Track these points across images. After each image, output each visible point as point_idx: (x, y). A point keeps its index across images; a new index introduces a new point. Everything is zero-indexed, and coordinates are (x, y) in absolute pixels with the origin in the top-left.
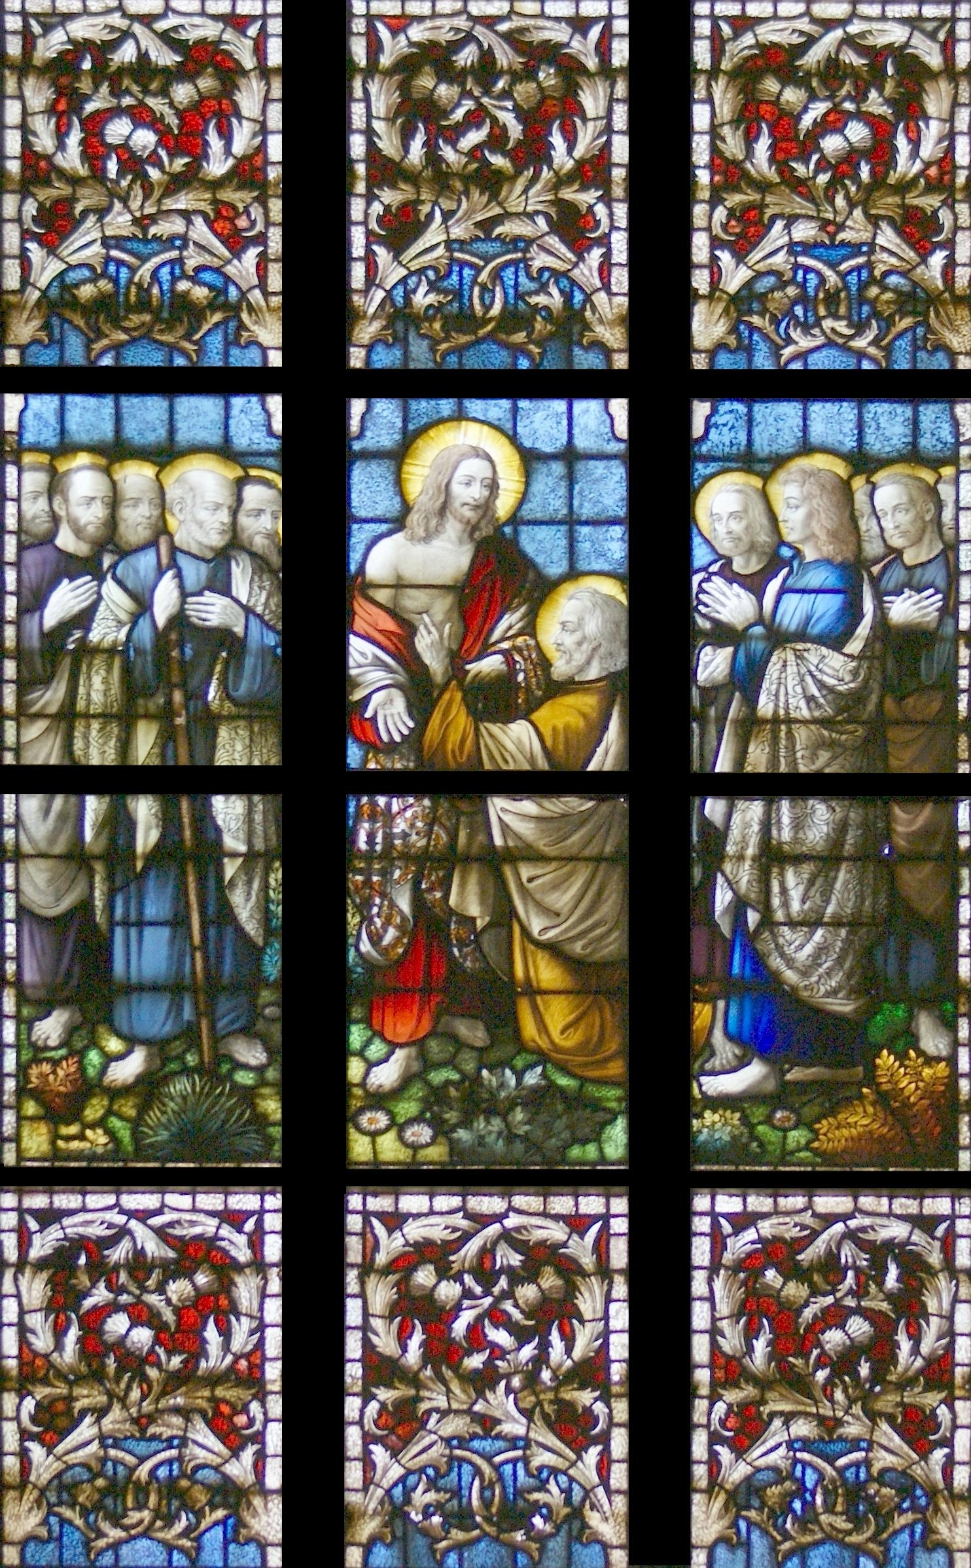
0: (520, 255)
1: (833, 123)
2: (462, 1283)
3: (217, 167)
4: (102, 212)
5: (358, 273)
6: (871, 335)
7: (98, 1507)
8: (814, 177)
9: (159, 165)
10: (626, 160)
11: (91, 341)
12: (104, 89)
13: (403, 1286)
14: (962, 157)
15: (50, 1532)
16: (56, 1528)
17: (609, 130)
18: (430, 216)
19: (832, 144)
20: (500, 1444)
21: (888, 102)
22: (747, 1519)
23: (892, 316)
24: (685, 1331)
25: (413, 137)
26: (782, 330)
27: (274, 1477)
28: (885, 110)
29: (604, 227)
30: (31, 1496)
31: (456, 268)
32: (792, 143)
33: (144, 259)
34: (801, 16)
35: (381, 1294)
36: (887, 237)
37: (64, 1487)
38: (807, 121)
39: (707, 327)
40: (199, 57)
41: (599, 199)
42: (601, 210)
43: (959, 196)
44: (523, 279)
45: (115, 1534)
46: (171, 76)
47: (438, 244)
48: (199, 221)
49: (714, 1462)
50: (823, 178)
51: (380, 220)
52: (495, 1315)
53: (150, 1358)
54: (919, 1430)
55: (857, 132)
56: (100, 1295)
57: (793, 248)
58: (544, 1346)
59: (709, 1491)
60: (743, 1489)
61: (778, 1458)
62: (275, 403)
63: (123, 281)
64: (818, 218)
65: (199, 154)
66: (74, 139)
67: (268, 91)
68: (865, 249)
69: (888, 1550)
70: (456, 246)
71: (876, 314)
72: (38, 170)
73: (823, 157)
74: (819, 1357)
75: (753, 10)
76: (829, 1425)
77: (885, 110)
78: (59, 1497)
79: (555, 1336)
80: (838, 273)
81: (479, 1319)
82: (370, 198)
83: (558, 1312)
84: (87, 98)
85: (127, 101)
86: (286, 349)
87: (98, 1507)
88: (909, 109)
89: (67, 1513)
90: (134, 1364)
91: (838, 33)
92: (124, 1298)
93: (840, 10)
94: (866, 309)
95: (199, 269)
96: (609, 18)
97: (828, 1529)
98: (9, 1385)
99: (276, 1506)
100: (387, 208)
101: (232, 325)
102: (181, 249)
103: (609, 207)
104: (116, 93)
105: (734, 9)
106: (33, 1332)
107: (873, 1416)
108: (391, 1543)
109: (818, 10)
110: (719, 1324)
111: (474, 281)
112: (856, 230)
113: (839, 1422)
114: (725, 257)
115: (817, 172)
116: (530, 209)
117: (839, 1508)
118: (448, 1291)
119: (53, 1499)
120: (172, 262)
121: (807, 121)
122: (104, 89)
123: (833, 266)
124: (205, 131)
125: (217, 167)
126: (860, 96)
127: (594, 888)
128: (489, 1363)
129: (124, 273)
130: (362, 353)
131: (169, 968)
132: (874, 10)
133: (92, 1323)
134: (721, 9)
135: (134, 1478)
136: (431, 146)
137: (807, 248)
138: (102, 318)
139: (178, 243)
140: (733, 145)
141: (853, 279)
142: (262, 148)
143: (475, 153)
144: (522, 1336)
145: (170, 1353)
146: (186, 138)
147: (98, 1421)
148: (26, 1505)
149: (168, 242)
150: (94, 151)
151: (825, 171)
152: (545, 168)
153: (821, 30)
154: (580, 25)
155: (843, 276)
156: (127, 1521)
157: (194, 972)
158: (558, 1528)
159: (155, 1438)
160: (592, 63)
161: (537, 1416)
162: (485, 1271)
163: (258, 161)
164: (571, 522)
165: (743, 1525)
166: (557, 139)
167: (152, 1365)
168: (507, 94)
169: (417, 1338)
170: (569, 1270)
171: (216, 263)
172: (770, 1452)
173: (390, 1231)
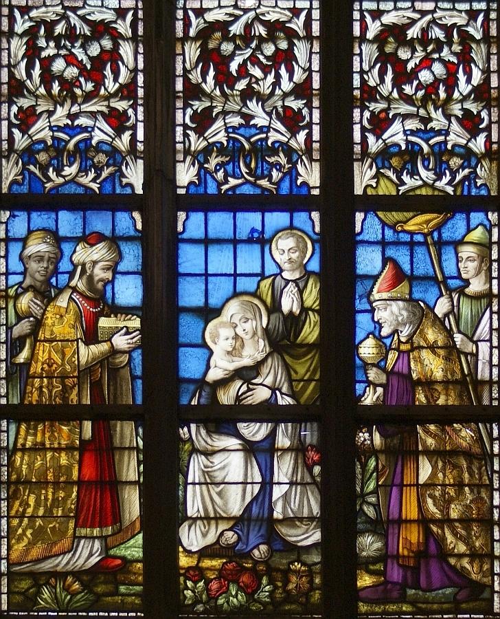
1: (426, 63)
2: (235, 43)
3: (111, 86)
4: (51, 113)
5: (179, 25)
8: (415, 94)
9: (80, 87)
12: (52, 44)
13: (204, 47)
14: (494, 82)
17: (310, 70)
19: (425, 76)
20: (253, 131)
24: (351, 72)
30: (14, 157)
32: (403, 76)
33: (72, 137)
34: (409, 8)
35: (192, 51)
36: (455, 127)
37: (29, 154)
38: (410, 65)
40: (101, 29)
43: (494, 103)
46: (86, 41)
48: (100, 118)
50: (421, 93)
52: (253, 60)
55: (438, 69)
56: (51, 51)
58: (278, 77)
59: (362, 160)
60: (378, 342)
65: (99, 82)
66: (37, 72)
68: (443, 132)
70: (231, 130)
72: (17, 88)
75: (383, 6)
76: (426, 120)
79: (283, 71)
80: (429, 145)
81: (245, 61)
83: (286, 58)
84: (43, 49)
85: (63, 52)
86: (144, 186)
88: (465, 58)
90: (68, 86)
91: (429, 17)
92: (63, 52)
93: (429, 6)
96: (310, 9)
97: (425, 179)
98: (3, 99)
104: (58, 47)
105: (372, 6)
107: (448, 117)
109: (418, 5)
112: (438, 120)
115: (417, 90)
117: (431, 167)
118: (227, 48)
121: (410, 65)
123: (427, 141)
125: (111, 86)
126: (439, 49)
128: (249, 85)
132: (447, 5)
133: (47, 63)
134: (366, 5)
135: (67, 148)
137: (413, 133)
142: (134, 80)
144: (266, 70)
145: (86, 81)
146: (95, 72)
147: (49, 117)
148: (11, 163)
150: (48, 77)
151: (421, 90)
153: (419, 16)
154: (296, 12)
155: (431, 147)
156: (63, 173)
157: (96, 492)
160: (302, 33)
161: (274, 116)
162: (247, 37)
163: (132, 87)
167: (77, 87)
169: (212, 73)
170: (291, 35)
173: (197, 17)
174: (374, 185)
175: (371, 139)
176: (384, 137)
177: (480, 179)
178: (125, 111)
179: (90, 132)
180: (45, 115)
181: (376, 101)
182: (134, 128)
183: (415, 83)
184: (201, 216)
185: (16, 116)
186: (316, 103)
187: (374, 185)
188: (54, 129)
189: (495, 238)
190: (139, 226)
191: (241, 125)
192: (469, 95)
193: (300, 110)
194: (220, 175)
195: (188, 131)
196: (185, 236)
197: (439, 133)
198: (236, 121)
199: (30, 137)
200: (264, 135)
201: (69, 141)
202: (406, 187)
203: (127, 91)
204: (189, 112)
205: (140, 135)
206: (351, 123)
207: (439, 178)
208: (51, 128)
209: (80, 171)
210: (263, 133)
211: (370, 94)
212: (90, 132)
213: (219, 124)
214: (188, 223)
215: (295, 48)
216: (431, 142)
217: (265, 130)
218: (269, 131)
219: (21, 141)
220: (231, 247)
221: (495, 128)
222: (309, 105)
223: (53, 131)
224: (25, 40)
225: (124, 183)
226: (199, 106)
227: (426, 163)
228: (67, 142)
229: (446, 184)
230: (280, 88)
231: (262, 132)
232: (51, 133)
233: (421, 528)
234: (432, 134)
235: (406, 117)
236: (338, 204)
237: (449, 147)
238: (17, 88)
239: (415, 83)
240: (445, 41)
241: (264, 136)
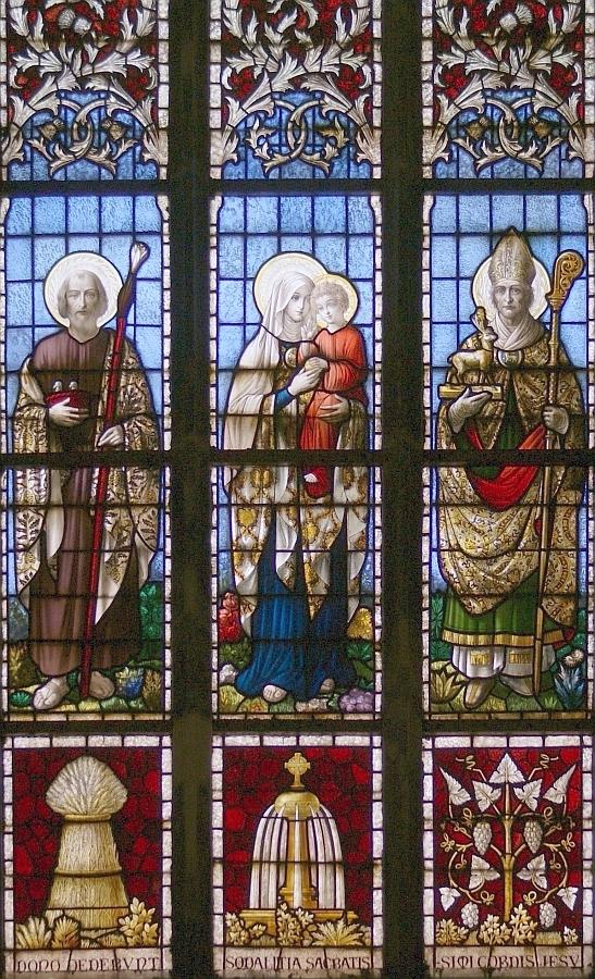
6: (532, 149)
7: (56, 139)
11: (50, 162)
15: (25, 156)
16: (29, 155)
17: (370, 18)
18: (261, 76)
20: (515, 95)
22: (455, 143)
23: (546, 137)
26: (477, 148)
27: (163, 118)
29: (369, 80)
31: (278, 111)
39: (431, 149)
41: (365, 62)
42: (366, 70)
44: (318, 119)
45: (65, 158)
49: (441, 790)
51: (230, 80)
53: (87, 38)
54: (561, 81)
61: (478, 100)
62: (164, 201)
63: (69, 120)
64: (499, 72)
67: (163, 377)
69: (544, 162)
70: (277, 96)
71: (536, 136)
73: (502, 30)
74: (500, 32)
78: (32, 134)
82: (224, 64)
87: (56, 139)
89: (35, 143)
94: (530, 134)
95: (115, 112)
99: (164, 140)
101: (138, 149)
103: (371, 66)
106: (15, 22)
108: (238, 162)
110: (438, 12)
111: (288, 119)
113: (514, 78)
114: (444, 100)
116: (323, 71)
119: (28, 135)
120: (99, 108)
124: (121, 19)
127: (371, 496)
129: (71, 115)
130: (219, 170)
136: (260, 30)
138: (57, 147)
139: (102, 96)
140: (446, 16)
143: (289, 33)
158: (340, 151)
159: (91, 91)
165: (454, 148)
172: (471, 96)
175: (234, 104)
176: (458, 101)
177: (574, 150)
180: (477, 77)
182: (370, 89)
184: (26, 202)
186: (377, 57)
191: (499, 89)
193: (360, 69)
194: (263, 152)
195: (12, 97)
198: (491, 82)
200: (316, 103)
201: (80, 111)
202: (59, 162)
203: (361, 43)
206: (206, 83)
207: (525, 149)
209: (91, 146)
213: (475, 86)
214: (223, 212)
216: (516, 105)
219: (23, 113)
220: (62, 240)
221: (590, 85)
222: (370, 61)
223: (60, 98)
226: (239, 64)
227: (509, 131)
229: (532, 156)
231: (315, 99)
232: (483, 101)
235: (483, 73)
236: (404, 193)
237: (109, 112)
238: (16, 44)
241: (102, 103)
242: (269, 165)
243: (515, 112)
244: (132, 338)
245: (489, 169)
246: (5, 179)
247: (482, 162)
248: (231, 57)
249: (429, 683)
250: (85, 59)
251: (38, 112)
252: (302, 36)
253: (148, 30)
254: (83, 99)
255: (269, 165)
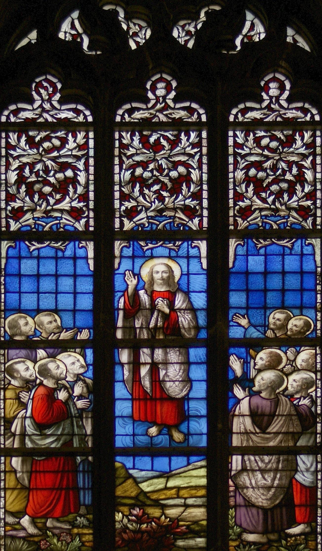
0: (172, 220)
10: (93, 199)
21: (293, 176)
25: (135, 187)
28: (292, 178)
47: (144, 218)
50: (272, 198)
57: (148, 217)
61: (31, 221)
70: (36, 219)
77: (292, 178)
100: (127, 208)
102: (59, 220)
122: (33, 175)
131: (205, 508)
141: (282, 226)
149: (56, 218)
151: (273, 195)
152: (180, 195)
164: (75, 276)
166: (184, 187)
168: (167, 175)
171: (72, 224)
174: (243, 244)
175: (12, 222)
178: (81, 208)
179: (287, 219)
181: (15, 201)
183: (268, 192)
185: (238, 211)
187: (243, 244)
188: (35, 219)
189: (3, 278)
190: (92, 268)
192: (303, 198)
193: (195, 207)
195: (237, 218)
196: (234, 270)
197: (284, 217)
199: (134, 222)
200: (58, 222)
204: (237, 207)
205: (319, 220)
208: (33, 218)
210: (285, 219)
211: (239, 197)
212: (59, 220)
215: (305, 174)
217: (59, 219)
218: (289, 218)
219: (14, 226)
224: (243, 172)
225: (193, 246)
228: (44, 227)
230: (296, 195)
231: (57, 220)
233: (238, 386)
234: (279, 218)
239: (268, 192)
240: (288, 169)
242: (145, 248)
243: (278, 225)
244: (161, 473)
245: (264, 249)
246: (201, 541)
247: (259, 246)
248: (125, 202)
249: (185, 499)
250: (48, 204)
251: (23, 226)
252: (165, 194)
253: (310, 141)
254: (161, 219)
255: (145, 248)
